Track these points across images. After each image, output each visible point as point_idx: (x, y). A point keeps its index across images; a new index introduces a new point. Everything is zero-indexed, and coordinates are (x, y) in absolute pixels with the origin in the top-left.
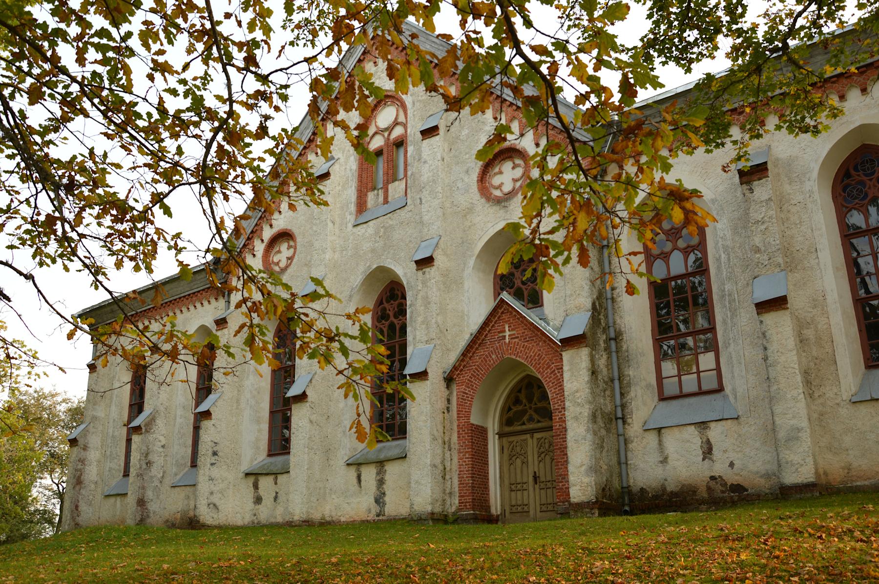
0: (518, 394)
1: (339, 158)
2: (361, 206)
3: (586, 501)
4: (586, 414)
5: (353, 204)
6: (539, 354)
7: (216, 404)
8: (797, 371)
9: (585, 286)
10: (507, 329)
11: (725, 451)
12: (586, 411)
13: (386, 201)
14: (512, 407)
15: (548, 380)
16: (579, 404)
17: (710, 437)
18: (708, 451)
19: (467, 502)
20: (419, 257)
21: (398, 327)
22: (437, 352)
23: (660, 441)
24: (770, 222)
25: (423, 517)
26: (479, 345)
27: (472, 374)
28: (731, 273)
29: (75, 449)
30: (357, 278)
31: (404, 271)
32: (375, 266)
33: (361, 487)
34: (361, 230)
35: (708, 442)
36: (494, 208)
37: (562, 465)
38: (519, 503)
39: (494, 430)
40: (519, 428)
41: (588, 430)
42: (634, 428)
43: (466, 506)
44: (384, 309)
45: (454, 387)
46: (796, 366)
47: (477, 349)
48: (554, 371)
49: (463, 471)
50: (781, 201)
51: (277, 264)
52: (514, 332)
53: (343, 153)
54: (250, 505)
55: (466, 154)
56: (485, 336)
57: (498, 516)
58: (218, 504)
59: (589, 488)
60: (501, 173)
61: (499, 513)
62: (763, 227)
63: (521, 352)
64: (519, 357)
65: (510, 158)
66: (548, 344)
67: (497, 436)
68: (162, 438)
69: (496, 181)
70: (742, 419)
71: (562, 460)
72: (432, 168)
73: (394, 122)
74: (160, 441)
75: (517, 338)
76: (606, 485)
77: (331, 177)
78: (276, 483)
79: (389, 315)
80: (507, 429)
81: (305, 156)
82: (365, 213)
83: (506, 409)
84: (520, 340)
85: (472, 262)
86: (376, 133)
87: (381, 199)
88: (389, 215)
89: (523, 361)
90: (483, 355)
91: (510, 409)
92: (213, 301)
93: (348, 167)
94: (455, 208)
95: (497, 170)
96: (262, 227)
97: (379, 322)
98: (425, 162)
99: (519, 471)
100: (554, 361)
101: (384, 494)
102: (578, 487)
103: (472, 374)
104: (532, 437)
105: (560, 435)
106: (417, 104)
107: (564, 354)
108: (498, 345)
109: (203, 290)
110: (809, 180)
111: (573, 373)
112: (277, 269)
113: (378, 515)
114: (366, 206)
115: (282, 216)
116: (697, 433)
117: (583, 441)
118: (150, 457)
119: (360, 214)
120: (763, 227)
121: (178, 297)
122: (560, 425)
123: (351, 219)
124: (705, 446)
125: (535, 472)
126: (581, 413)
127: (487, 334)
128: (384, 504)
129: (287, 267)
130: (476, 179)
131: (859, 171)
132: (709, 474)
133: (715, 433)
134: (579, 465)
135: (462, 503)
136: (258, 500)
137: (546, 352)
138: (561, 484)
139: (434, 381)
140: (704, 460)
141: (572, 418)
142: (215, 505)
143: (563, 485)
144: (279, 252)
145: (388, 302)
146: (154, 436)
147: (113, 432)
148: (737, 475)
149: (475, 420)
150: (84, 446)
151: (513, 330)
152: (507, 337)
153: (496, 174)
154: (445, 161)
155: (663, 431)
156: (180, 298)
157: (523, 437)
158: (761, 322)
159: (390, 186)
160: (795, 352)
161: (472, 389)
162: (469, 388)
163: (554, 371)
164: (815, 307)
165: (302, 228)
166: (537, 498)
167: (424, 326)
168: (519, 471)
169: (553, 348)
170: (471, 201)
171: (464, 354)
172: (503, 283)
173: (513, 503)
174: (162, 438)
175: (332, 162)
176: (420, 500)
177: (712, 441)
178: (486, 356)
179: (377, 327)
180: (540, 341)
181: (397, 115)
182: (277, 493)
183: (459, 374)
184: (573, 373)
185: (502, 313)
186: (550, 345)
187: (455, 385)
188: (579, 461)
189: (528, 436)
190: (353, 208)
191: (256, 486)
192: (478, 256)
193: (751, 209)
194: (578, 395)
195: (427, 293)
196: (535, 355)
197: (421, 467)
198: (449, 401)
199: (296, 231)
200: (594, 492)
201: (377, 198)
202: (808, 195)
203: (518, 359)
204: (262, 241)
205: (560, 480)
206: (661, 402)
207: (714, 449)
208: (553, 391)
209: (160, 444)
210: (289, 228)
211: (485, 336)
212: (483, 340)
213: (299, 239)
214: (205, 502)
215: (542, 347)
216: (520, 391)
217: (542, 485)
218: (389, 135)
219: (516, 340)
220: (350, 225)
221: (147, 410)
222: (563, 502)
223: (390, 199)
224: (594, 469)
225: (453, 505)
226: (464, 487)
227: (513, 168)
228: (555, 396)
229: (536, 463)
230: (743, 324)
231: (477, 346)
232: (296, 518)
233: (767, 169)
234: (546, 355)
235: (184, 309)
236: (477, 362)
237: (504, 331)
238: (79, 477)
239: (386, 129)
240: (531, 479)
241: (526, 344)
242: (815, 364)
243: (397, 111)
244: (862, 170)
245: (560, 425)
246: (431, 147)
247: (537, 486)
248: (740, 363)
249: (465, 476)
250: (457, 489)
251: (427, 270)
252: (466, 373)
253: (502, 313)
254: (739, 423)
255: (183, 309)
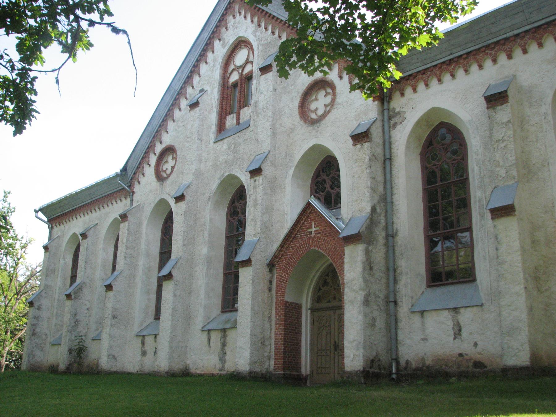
0: (326, 278)
1: (207, 90)
2: (221, 127)
4: (359, 299)
5: (214, 126)
7: (117, 279)
8: (520, 269)
9: (366, 193)
10: (313, 226)
11: (471, 333)
12: (360, 297)
13: (238, 123)
14: (322, 288)
16: (354, 290)
17: (460, 321)
18: (458, 332)
20: (252, 168)
21: (333, 196)
22: (262, 243)
23: (423, 322)
24: (508, 140)
26: (293, 239)
27: (287, 261)
28: (481, 182)
29: (32, 309)
30: (214, 184)
31: (245, 178)
32: (226, 174)
33: (210, 347)
34: (219, 144)
35: (458, 324)
36: (309, 128)
39: (306, 307)
41: (359, 312)
42: (403, 310)
44: (235, 207)
45: (275, 272)
46: (520, 265)
47: (291, 241)
49: (278, 339)
50: (522, 121)
51: (165, 171)
52: (318, 229)
53: (210, 86)
54: (139, 357)
55: (292, 85)
56: (298, 232)
57: (307, 376)
58: (116, 356)
60: (316, 99)
61: (308, 373)
62: (502, 145)
65: (324, 88)
67: (309, 311)
68: (87, 303)
69: (313, 106)
70: (485, 307)
72: (266, 97)
73: (245, 62)
74: (86, 305)
75: (319, 233)
76: (375, 358)
77: (200, 105)
78: (156, 341)
79: (238, 212)
80: (318, 306)
81: (185, 89)
82: (223, 132)
83: (318, 289)
85: (291, 172)
86: (234, 70)
87: (235, 121)
88: (238, 134)
89: (323, 252)
91: (320, 289)
92: (123, 199)
93: (213, 98)
94: (283, 128)
95: (314, 97)
96: (155, 144)
97: (231, 217)
98: (262, 93)
101: (225, 353)
106: (261, 47)
107: (345, 248)
108: (306, 238)
109: (117, 191)
110: (545, 104)
112: (165, 175)
113: (221, 370)
114: (225, 127)
115: (169, 135)
116: (450, 317)
118: (78, 317)
119: (220, 133)
120: (502, 145)
121: (100, 196)
123: (212, 136)
124: (456, 328)
126: (355, 298)
127: (299, 230)
128: (225, 361)
129: (172, 172)
130: (298, 105)
132: (458, 351)
133: (465, 316)
135: (276, 364)
136: (144, 353)
139: (258, 267)
140: (455, 339)
142: (114, 356)
144: (167, 162)
145: (238, 201)
146: (81, 301)
147: (59, 296)
148: (480, 353)
149: (289, 298)
150: (39, 307)
151: (317, 227)
152: (313, 233)
153: (313, 101)
154: (277, 91)
155: (425, 313)
156: (102, 197)
157: (328, 312)
158: (495, 226)
159: (242, 111)
160: (519, 253)
161: (287, 274)
162: (285, 272)
164: (546, 212)
165: (181, 144)
167: (253, 223)
170: (293, 123)
171: (282, 246)
172: (333, 183)
173: (319, 365)
174: (87, 303)
175: (203, 93)
177: (462, 324)
178: (298, 247)
179: (230, 221)
181: (248, 56)
182: (156, 349)
185: (310, 213)
187: (276, 270)
190: (214, 128)
191: (143, 343)
192: (297, 166)
193: (494, 130)
195: (256, 196)
196: (331, 248)
198: (271, 282)
199: (177, 146)
200: (362, 364)
201: (233, 120)
202: (543, 117)
203: (320, 250)
204: (155, 154)
206: (428, 289)
207: (462, 331)
209: (86, 308)
210: (173, 144)
211: (298, 232)
213: (179, 153)
214: (106, 354)
216: (327, 275)
218: (242, 71)
219: (319, 235)
220: (212, 142)
221: (79, 280)
223: (241, 121)
224: (367, 345)
225: (271, 365)
227: (325, 96)
230: (489, 226)
231: (291, 239)
232: (162, 370)
233: (507, 96)
234: (339, 248)
235: (105, 206)
236: (290, 252)
238: (34, 330)
239: (240, 67)
240: (332, 347)
241: (326, 238)
242: (544, 262)
243: (248, 52)
246: (266, 81)
247: (336, 353)
248: (485, 259)
250: (273, 353)
251: (257, 178)
252: (283, 261)
253: (310, 213)
254: (483, 310)
255: (104, 206)
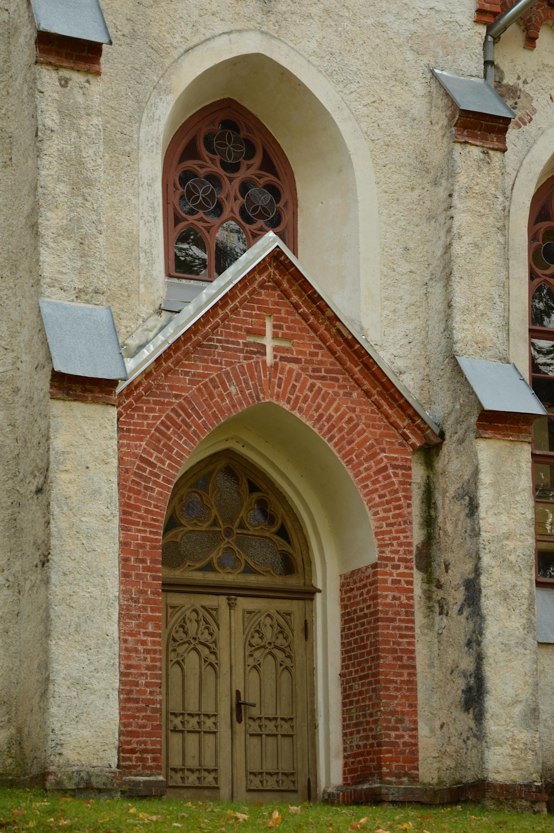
3: (520, 781)
6: (350, 420)
15: (371, 487)
19: (146, 751)
25: (96, 782)
27: (168, 417)
37: (397, 689)
38: (192, 763)
40: (198, 577)
43: (142, 760)
48: (385, 468)
49: (137, 667)
59: (530, 756)
63: (305, 400)
64: (301, 410)
66: (376, 403)
71: (399, 679)
75: (296, 361)
84: (305, 370)
90: (204, 376)
99: (192, 684)
100: (384, 445)
102: (506, 750)
103: (168, 417)
104: (231, 606)
105: (393, 620)
111: (499, 493)
117: (521, 650)
122: (394, 598)
125: (238, 693)
126: (514, 586)
131: (544, 240)
134: (509, 700)
137: (367, 418)
138: (393, 734)
141: (496, 593)
143: (397, 737)
151: (285, 337)
157: (210, 601)
163: (385, 468)
166: (240, 756)
168: (192, 684)
169: (388, 417)
173: (256, 768)
176: (86, 733)
180: (353, 388)
183: (130, 405)
184: (499, 493)
186: (379, 407)
188: (511, 692)
189: (223, 600)
194: (510, 544)
197: (92, 643)
205: (393, 724)
208: (382, 514)
212: (205, 337)
215: (359, 403)
217: (254, 727)
219: (295, 366)
222: (398, 776)
226: (139, 710)
228: (385, 528)
229: (239, 668)
234: (368, 426)
237: (262, 334)
241: (318, 383)
244: (188, 190)
245: (394, 598)
247: (240, 728)
249: (142, 681)
252: (150, 410)
